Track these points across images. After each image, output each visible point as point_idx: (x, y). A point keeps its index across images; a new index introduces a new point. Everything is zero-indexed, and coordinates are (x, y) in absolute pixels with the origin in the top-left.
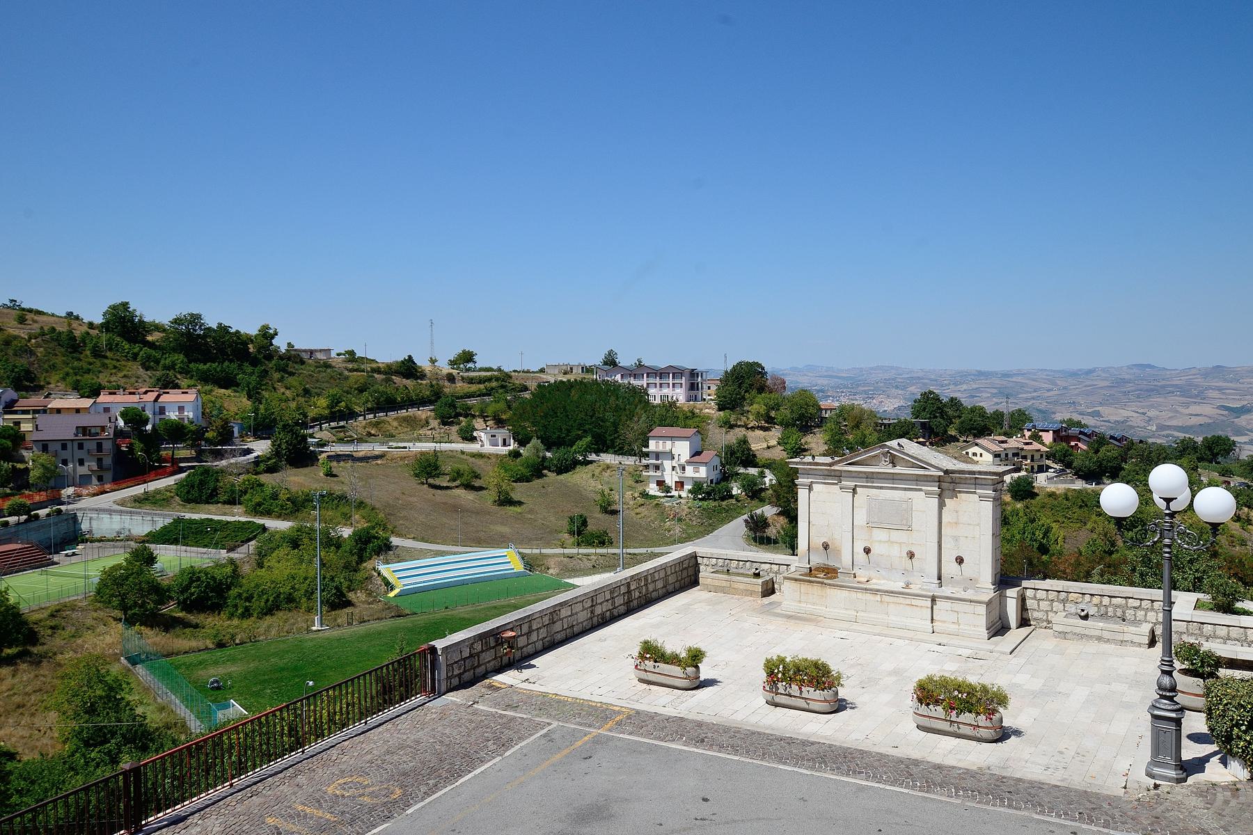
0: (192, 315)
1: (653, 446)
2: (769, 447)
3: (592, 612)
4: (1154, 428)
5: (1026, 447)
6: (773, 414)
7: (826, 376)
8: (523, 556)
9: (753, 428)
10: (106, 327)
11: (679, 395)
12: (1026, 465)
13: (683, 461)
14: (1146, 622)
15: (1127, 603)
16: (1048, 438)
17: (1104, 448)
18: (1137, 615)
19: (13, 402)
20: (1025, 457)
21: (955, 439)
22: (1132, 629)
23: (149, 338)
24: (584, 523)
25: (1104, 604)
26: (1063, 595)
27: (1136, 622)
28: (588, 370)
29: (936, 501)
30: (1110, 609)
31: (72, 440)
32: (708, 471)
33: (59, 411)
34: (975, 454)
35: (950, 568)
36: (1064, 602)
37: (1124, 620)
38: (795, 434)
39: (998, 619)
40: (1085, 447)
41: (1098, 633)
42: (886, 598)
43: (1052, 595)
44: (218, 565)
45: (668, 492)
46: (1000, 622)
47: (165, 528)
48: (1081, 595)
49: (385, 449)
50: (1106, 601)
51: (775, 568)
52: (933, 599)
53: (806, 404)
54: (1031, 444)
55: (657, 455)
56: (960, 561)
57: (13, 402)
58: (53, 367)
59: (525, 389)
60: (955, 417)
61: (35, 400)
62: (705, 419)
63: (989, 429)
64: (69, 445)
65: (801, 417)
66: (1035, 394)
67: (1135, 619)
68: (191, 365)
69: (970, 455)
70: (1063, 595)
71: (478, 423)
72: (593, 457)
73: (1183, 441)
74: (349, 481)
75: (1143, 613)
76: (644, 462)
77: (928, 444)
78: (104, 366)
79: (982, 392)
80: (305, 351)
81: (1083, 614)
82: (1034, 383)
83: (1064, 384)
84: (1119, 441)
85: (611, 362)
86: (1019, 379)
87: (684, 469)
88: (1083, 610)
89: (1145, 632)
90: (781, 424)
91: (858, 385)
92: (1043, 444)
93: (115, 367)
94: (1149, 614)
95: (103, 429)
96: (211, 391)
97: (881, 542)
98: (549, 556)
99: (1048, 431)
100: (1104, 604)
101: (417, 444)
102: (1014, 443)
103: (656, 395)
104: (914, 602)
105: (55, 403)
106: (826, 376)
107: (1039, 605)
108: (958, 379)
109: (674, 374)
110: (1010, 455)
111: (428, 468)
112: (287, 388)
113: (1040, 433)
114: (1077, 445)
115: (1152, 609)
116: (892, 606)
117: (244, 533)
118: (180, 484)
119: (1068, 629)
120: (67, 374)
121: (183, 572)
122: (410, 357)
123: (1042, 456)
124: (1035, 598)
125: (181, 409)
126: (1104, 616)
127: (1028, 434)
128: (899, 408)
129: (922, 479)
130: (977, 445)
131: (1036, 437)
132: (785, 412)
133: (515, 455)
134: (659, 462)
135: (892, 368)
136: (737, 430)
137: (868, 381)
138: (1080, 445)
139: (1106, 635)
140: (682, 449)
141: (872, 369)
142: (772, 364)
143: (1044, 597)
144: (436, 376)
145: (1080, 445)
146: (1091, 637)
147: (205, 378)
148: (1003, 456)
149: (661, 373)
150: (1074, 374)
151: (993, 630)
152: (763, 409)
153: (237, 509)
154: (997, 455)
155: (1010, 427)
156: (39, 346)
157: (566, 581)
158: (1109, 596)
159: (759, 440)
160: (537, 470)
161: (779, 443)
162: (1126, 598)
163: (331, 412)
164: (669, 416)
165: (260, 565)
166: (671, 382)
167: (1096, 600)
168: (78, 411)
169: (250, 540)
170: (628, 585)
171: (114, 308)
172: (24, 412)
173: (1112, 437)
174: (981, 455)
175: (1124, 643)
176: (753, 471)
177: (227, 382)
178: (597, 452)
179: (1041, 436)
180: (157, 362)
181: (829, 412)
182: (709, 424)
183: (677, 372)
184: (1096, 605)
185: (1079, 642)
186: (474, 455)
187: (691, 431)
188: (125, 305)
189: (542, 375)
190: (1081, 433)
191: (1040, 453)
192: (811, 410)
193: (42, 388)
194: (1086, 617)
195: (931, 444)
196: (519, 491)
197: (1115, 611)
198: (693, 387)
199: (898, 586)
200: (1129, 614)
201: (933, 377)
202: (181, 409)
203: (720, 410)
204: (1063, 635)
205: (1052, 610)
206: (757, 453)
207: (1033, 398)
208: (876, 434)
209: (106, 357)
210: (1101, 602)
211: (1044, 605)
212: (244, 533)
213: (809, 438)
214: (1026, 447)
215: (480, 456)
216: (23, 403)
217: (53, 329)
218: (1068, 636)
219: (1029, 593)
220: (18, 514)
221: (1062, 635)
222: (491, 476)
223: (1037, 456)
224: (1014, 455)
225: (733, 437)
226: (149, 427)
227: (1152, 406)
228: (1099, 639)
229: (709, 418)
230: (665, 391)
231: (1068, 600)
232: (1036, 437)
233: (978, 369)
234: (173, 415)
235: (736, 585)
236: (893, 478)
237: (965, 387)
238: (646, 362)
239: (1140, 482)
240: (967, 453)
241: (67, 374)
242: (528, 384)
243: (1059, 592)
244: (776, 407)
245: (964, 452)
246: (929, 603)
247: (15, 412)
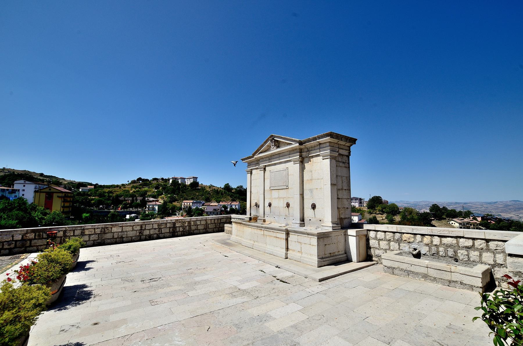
2: (383, 219)
5: (471, 222)
6: (384, 210)
7: (406, 204)
9: (378, 214)
10: (224, 189)
12: (471, 227)
14: (482, 263)
15: (458, 243)
16: (479, 219)
17: (502, 223)
18: (471, 255)
19: (204, 204)
20: (471, 225)
21: (445, 219)
22: (461, 268)
23: (233, 191)
25: (434, 243)
26: (397, 236)
27: (469, 262)
29: (298, 166)
30: (441, 249)
31: (212, 212)
33: (212, 206)
34: (452, 223)
35: (309, 213)
36: (399, 241)
37: (456, 260)
38: (391, 216)
39: (343, 252)
40: (494, 223)
41: (423, 270)
43: (389, 236)
46: (345, 255)
48: (412, 236)
52: (288, 233)
53: (394, 207)
54: (473, 221)
56: (314, 207)
57: (204, 204)
58: (213, 197)
61: (208, 203)
62: (364, 211)
64: (212, 213)
65: (393, 211)
66: (476, 209)
67: (469, 259)
68: (240, 197)
69: (451, 224)
70: (397, 236)
75: (477, 253)
77: (435, 220)
78: (223, 197)
79: (457, 208)
81: (415, 253)
82: (476, 206)
83: (487, 206)
84: (508, 221)
86: (470, 205)
88: (415, 249)
89: (476, 273)
90: (386, 213)
91: (417, 206)
92: (478, 221)
93: (225, 197)
94: (485, 255)
95: (219, 209)
96: (243, 202)
98: (116, 201)
99: (479, 217)
100: (434, 243)
102: (466, 220)
105: (211, 204)
106: (406, 204)
107: (379, 244)
108: (449, 204)
109: (355, 199)
110: (465, 224)
113: (476, 218)
114: (491, 222)
115: (488, 250)
116: (268, 237)
119: (396, 265)
120: (216, 198)
123: (477, 225)
124: (376, 238)
125: (236, 206)
126: (435, 255)
127: (471, 218)
129: (292, 153)
130: (453, 220)
131: (475, 218)
135: (427, 201)
136: (373, 214)
137: (420, 205)
138: (492, 222)
139: (432, 273)
141: (421, 201)
142: (384, 198)
143: (383, 237)
145: (492, 222)
146: (417, 274)
148: (463, 224)
150: (490, 203)
151: (358, 261)
152: (381, 209)
154: (460, 224)
155: (465, 215)
156: (212, 193)
158: (439, 236)
159: (380, 217)
161: (386, 218)
162: (456, 237)
166: (354, 201)
167: (427, 240)
168: (215, 206)
171: (226, 184)
172: (206, 206)
173: (504, 219)
174: (455, 224)
175: (453, 284)
179: (477, 218)
180: (233, 196)
181: (401, 210)
182: (365, 213)
184: (427, 245)
185: (406, 278)
188: (228, 184)
190: (492, 218)
191: (476, 224)
193: (211, 201)
194: (418, 256)
195: (437, 220)
197: (446, 251)
198: (360, 203)
200: (462, 254)
201: (440, 204)
202: (236, 206)
203: (368, 209)
206: (379, 221)
207: (476, 210)
208: (417, 216)
209: (223, 195)
210: (432, 242)
211: (383, 244)
213: (395, 217)
214: (471, 222)
216: (206, 204)
217: (215, 189)
218: (396, 271)
219: (372, 234)
221: (390, 270)
223: (475, 225)
224: (467, 224)
225: (371, 216)
226: (229, 209)
227: (521, 213)
228: (425, 276)
229: (365, 211)
231: (402, 240)
232: (475, 218)
233: (456, 201)
236: (279, 155)
237: (451, 207)
240: (450, 223)
241: (216, 198)
243: (394, 233)
244: (385, 208)
245: (448, 223)
246: (284, 236)
247: (204, 206)
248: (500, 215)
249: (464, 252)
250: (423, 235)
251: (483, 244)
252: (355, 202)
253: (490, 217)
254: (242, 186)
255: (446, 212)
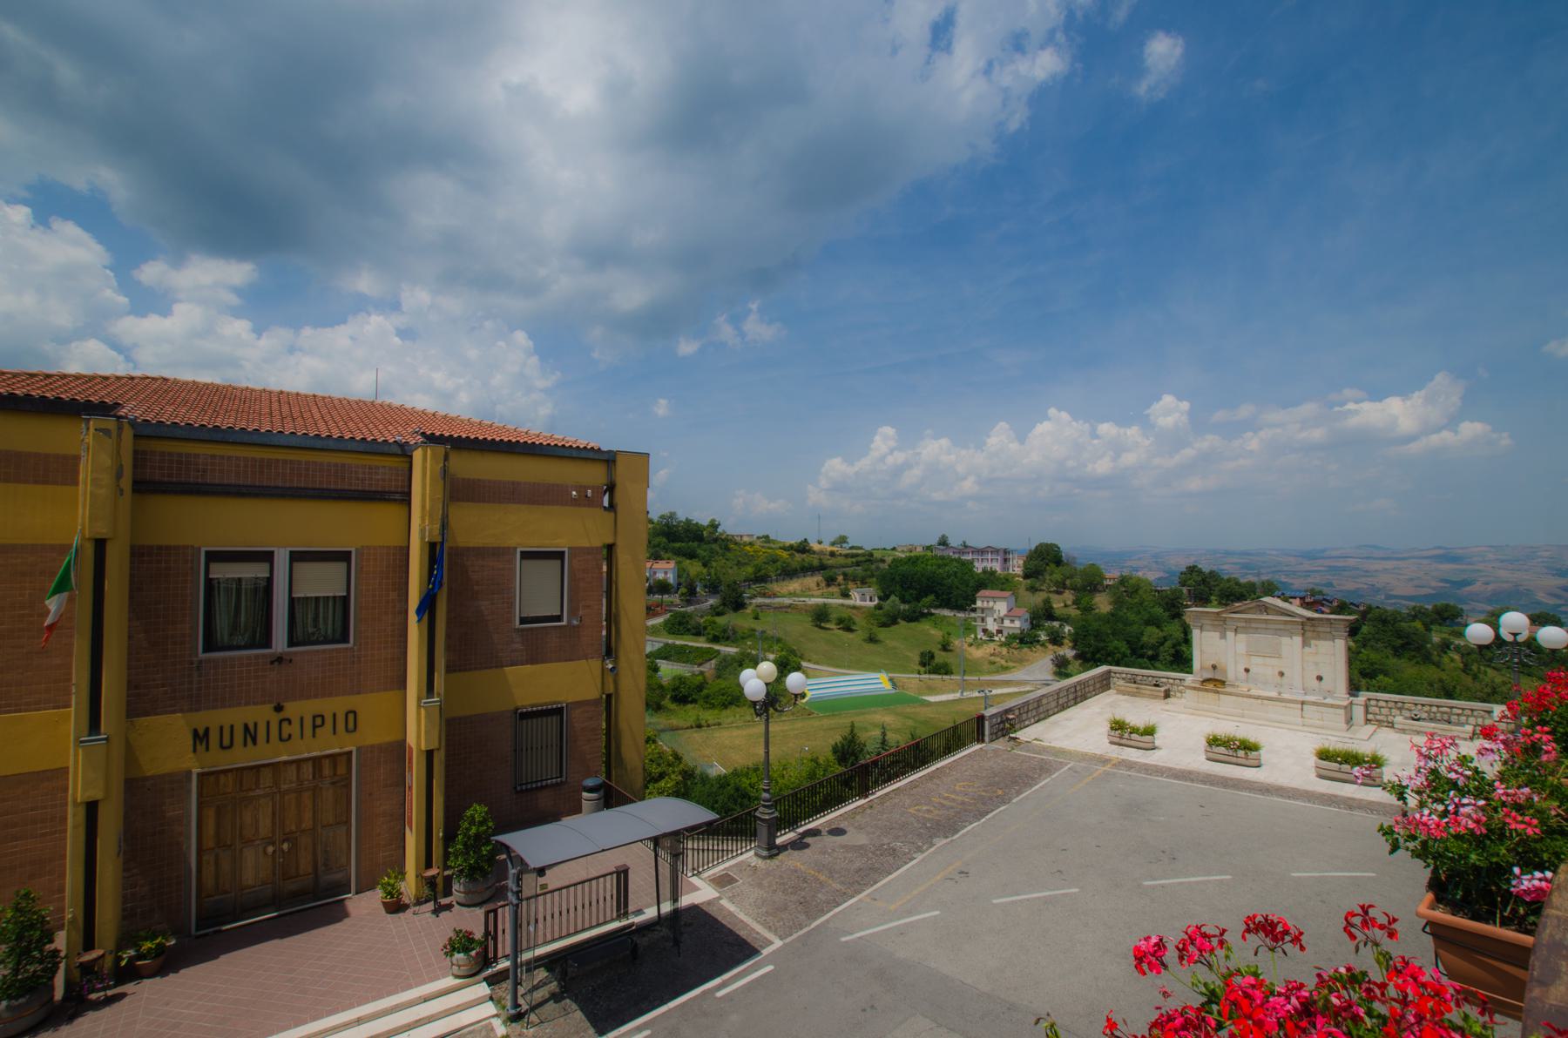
0: (671, 513)
1: (979, 604)
3: (1058, 702)
4: (1383, 597)
8: (891, 680)
11: (997, 566)
13: (1002, 614)
24: (932, 657)
27: (1462, 724)
28: (929, 548)
30: (1438, 715)
32: (1021, 624)
36: (1400, 709)
42: (1265, 702)
43: (1391, 705)
44: (694, 675)
45: (991, 637)
47: (659, 649)
49: (791, 602)
50: (1434, 709)
51: (1171, 681)
55: (983, 610)
59: (883, 561)
60: (1215, 586)
63: (1244, 596)
70: (1400, 705)
71: (851, 585)
72: (933, 611)
73: (1414, 608)
74: (766, 625)
75: (1465, 718)
76: (973, 615)
80: (737, 536)
85: (943, 542)
87: (1003, 620)
88: (1416, 715)
97: (1257, 664)
99: (1295, 598)
101: (812, 599)
103: (979, 567)
104: (1288, 705)
111: (820, 616)
112: (727, 560)
115: (1472, 716)
117: (705, 656)
118: (666, 623)
121: (674, 678)
122: (806, 539)
125: (666, 573)
128: (1159, 579)
132: (1078, 581)
133: (879, 607)
134: (984, 615)
140: (1001, 607)
142: (1066, 547)
144: (822, 553)
147: (679, 553)
149: (982, 552)
153: (702, 639)
157: (924, 698)
160: (891, 620)
163: (756, 577)
164: (988, 581)
165: (719, 677)
169: (711, 660)
170: (1075, 686)
176: (1056, 624)
177: (692, 556)
178: (937, 607)
183: (995, 551)
184: (1426, 712)
186: (849, 607)
187: (1007, 594)
189: (894, 553)
190: (1324, 599)
192: (1098, 579)
196: (882, 633)
199: (1274, 694)
200: (1454, 718)
202: (666, 573)
204: (1403, 731)
205: (1391, 715)
212: (705, 656)
215: (854, 607)
218: (1407, 732)
220: (1187, 605)
222: (860, 621)
230: (985, 564)
234: (660, 576)
235: (1144, 692)
238: (968, 544)
239: (1493, 620)
242: (886, 558)
248: (1330, 585)
249: (1456, 717)
250: (1423, 705)
251: (1469, 713)
252: (992, 560)
253: (1321, 597)
254: (675, 513)
255: (1218, 585)
